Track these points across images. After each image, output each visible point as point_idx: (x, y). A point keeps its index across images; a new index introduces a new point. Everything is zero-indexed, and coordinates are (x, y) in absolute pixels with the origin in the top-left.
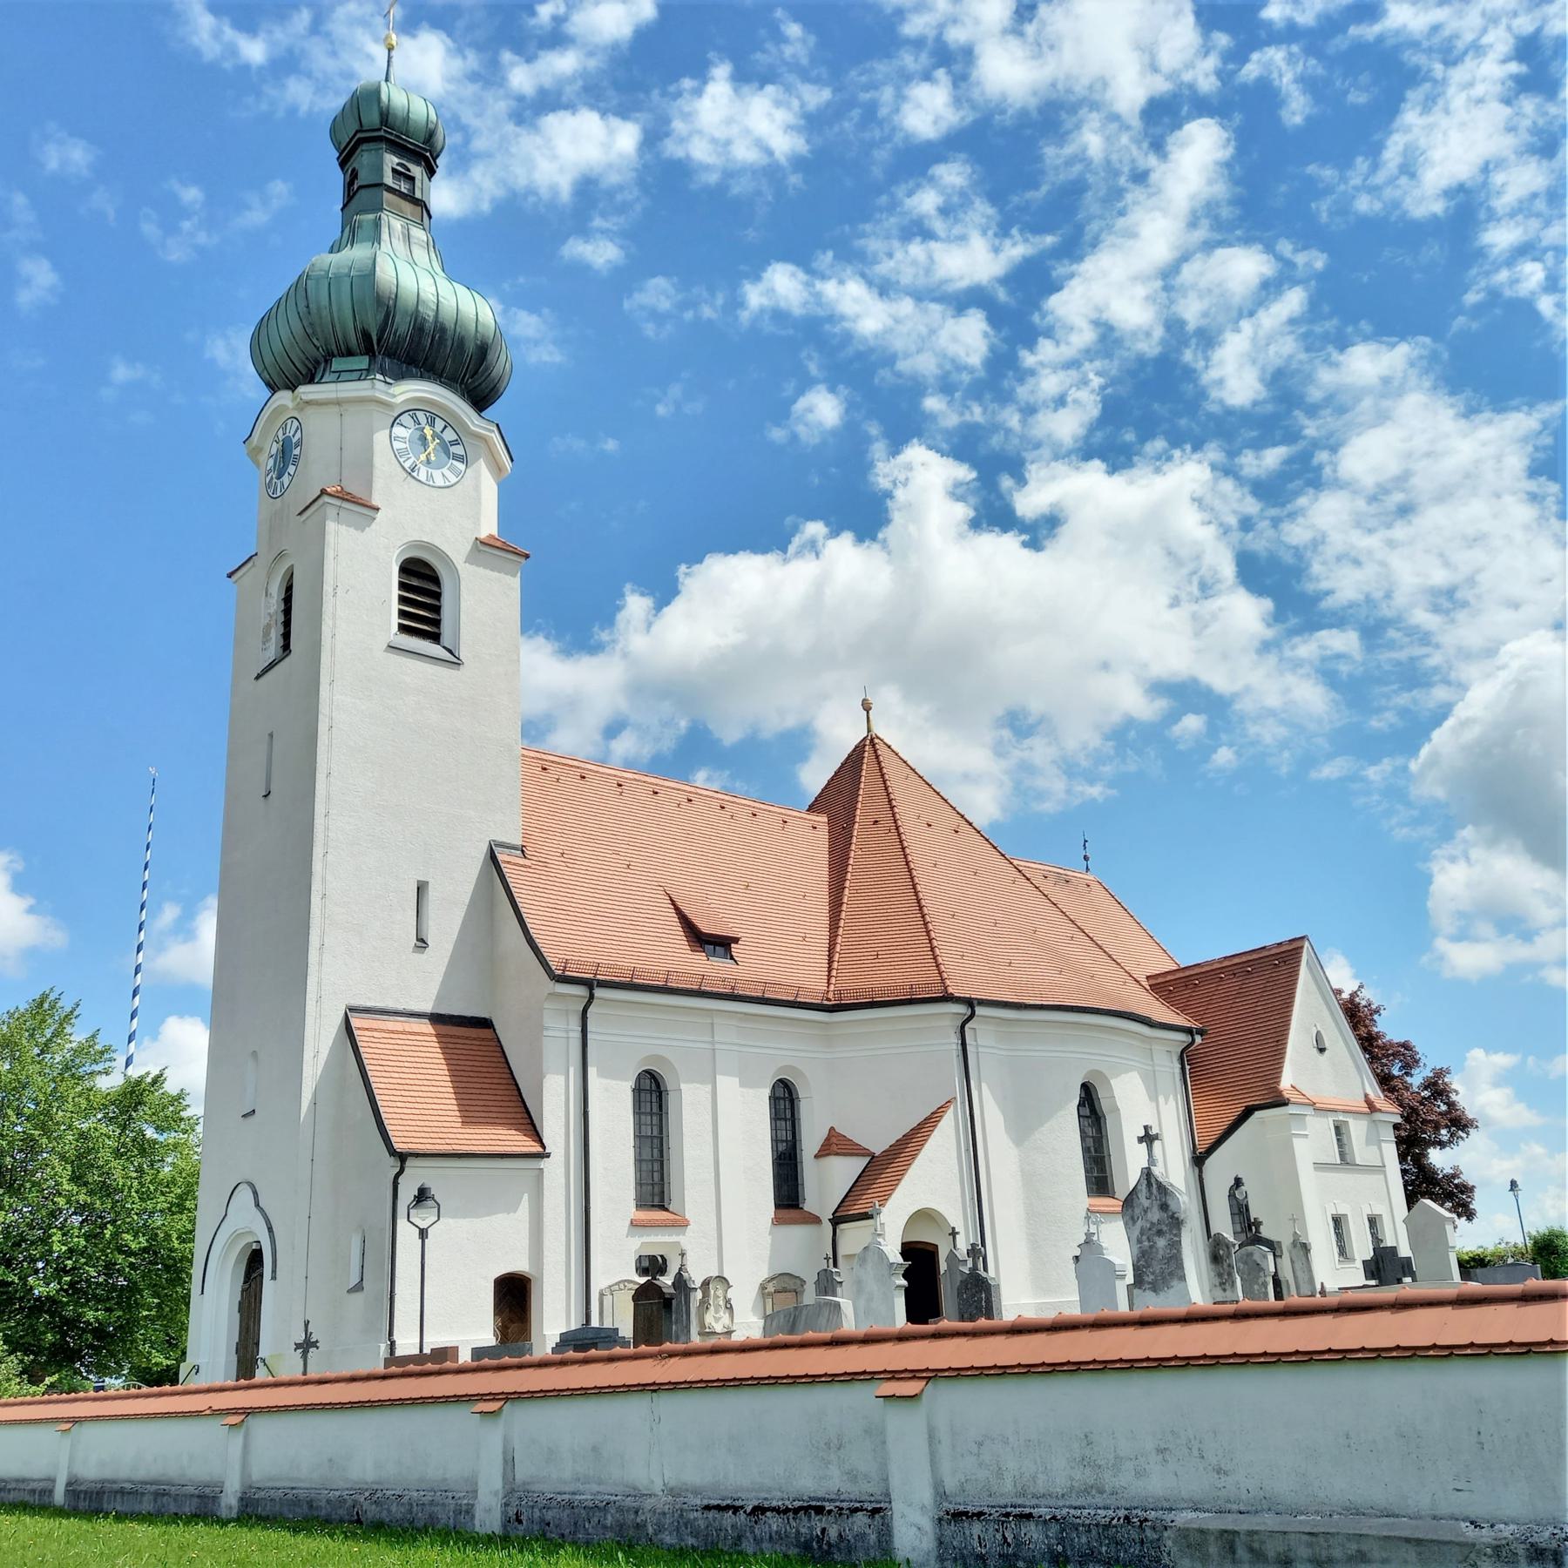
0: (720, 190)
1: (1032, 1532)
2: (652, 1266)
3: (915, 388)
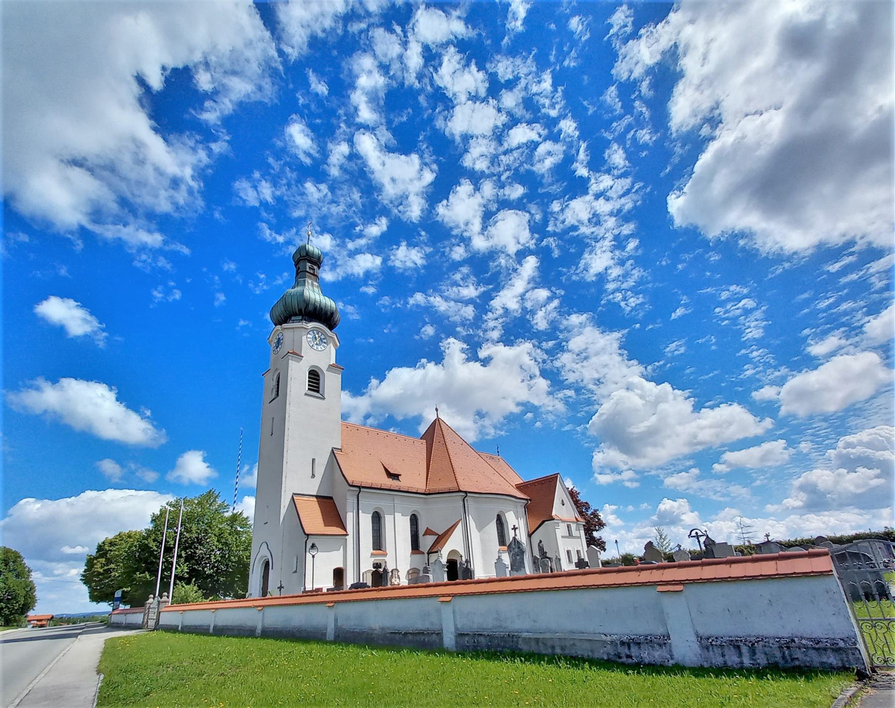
0: (402, 274)
1: (482, 639)
2: (377, 566)
3: (455, 325)
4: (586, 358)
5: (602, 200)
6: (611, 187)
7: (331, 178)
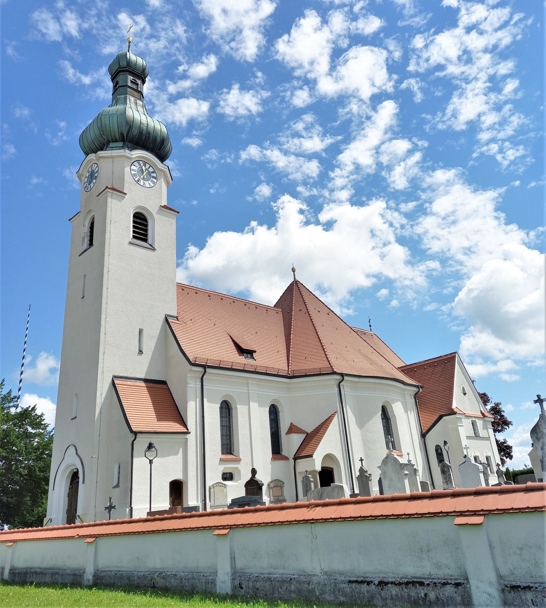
0: (234, 122)
4: (454, 222)
5: (474, 34)
6: (486, 19)
7: (151, 9)
